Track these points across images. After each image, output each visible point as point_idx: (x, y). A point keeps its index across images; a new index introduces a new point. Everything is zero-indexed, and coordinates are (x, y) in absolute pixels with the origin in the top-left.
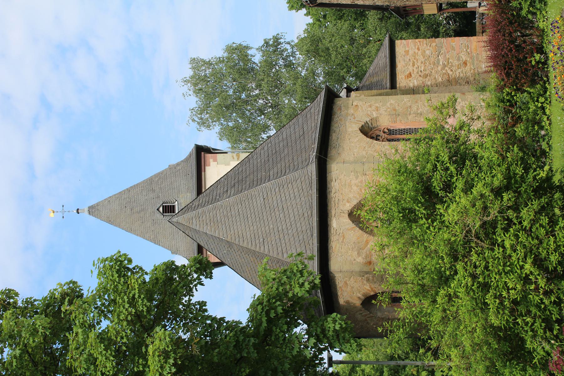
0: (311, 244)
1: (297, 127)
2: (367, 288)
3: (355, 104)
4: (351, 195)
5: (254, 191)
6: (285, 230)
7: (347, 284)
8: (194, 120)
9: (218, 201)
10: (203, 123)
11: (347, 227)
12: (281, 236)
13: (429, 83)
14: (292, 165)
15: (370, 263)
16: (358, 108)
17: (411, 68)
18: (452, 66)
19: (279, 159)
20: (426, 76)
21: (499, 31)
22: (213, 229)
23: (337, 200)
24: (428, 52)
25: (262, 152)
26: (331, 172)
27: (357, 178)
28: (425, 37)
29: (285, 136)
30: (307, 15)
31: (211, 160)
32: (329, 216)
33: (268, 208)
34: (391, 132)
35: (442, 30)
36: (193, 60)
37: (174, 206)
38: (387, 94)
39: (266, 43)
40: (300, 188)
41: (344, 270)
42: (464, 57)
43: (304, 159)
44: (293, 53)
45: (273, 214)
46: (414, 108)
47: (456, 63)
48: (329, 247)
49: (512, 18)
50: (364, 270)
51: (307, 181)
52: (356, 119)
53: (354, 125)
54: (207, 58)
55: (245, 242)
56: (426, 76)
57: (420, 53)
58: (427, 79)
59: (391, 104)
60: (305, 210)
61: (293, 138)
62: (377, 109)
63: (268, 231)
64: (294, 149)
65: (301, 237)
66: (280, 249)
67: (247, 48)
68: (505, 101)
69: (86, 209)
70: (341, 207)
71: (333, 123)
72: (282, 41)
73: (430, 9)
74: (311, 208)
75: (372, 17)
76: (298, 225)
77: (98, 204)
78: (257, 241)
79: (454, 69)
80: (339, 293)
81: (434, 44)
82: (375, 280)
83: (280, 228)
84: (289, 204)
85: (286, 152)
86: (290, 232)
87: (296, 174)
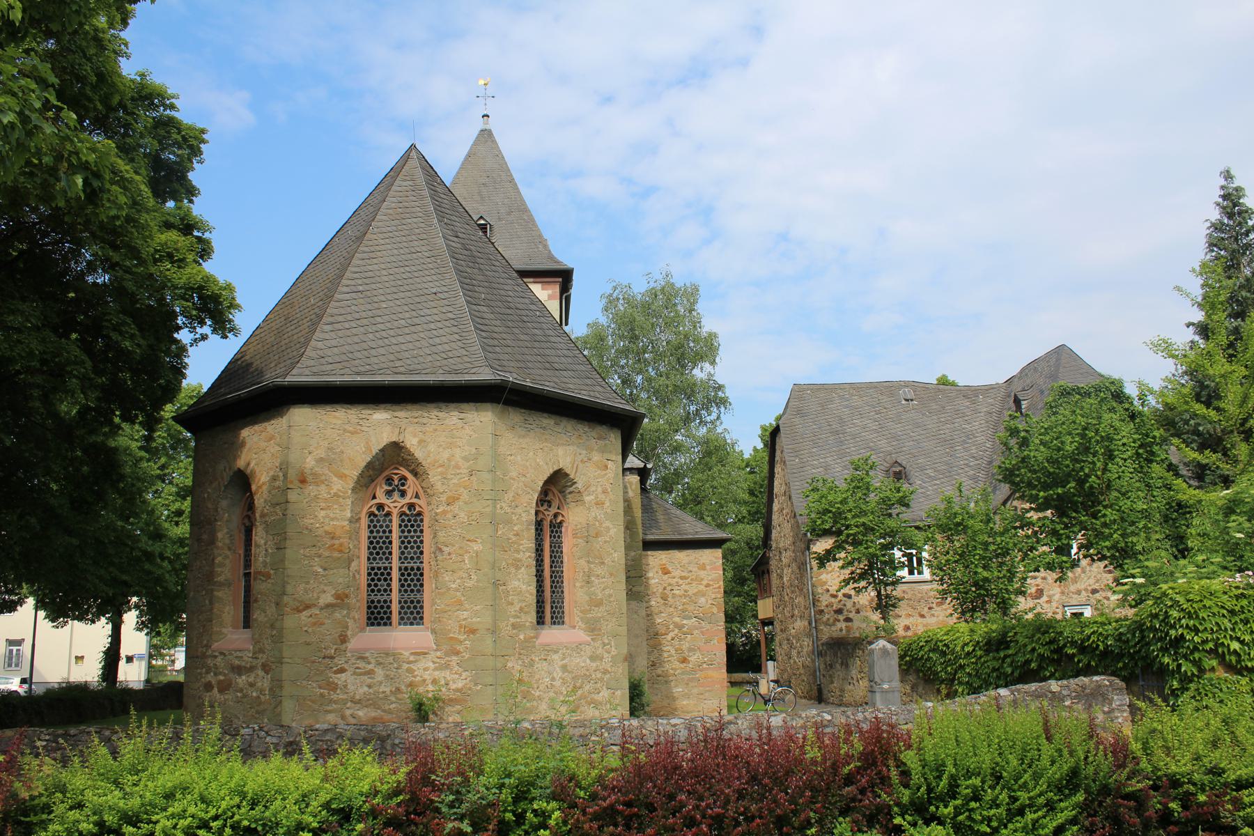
0: (342, 372)
1: (569, 360)
2: (262, 480)
4: (432, 448)
5: (452, 278)
6: (374, 328)
7: (271, 439)
8: (615, 288)
9: (439, 221)
10: (611, 302)
11: (373, 439)
12: (365, 322)
13: (653, 603)
14: (496, 342)
15: (303, 481)
16: (600, 475)
17: (677, 573)
18: (680, 640)
19: (510, 324)
20: (665, 598)
21: (754, 779)
22: (390, 211)
23: (425, 421)
24: (702, 600)
25: (527, 301)
26: (477, 410)
27: (466, 459)
28: (726, 603)
29: (553, 339)
30: (755, 449)
32: (394, 407)
33: (418, 300)
34: (556, 527)
35: (735, 626)
36: (696, 289)
38: (629, 526)
39: (720, 388)
40: (450, 354)
41: (293, 432)
42: (694, 658)
43: (505, 363)
44: (706, 423)
45: (406, 308)
46: (599, 570)
47: (685, 646)
48: (337, 406)
49: (796, 822)
50: (290, 471)
51: (461, 366)
52: (581, 465)
53: (568, 459)
54: (700, 307)
55: (361, 262)
56: (665, 598)
57: (702, 587)
58: (659, 600)
59: (608, 529)
60: (409, 362)
61: (548, 352)
62: (599, 504)
63: (375, 299)
64: (526, 351)
65: (358, 355)
66: (341, 319)
67: (713, 363)
68: (522, 805)
69: (487, 127)
70: (410, 429)
72: (722, 409)
73: (765, 608)
74: (411, 372)
75: (754, 531)
76: (382, 351)
77: (494, 142)
78: (360, 282)
79: (676, 642)
80: (256, 427)
81: (715, 610)
82: (274, 492)
83: (379, 319)
84: (422, 335)
85: (522, 337)
86: (371, 336)
87: (477, 348)
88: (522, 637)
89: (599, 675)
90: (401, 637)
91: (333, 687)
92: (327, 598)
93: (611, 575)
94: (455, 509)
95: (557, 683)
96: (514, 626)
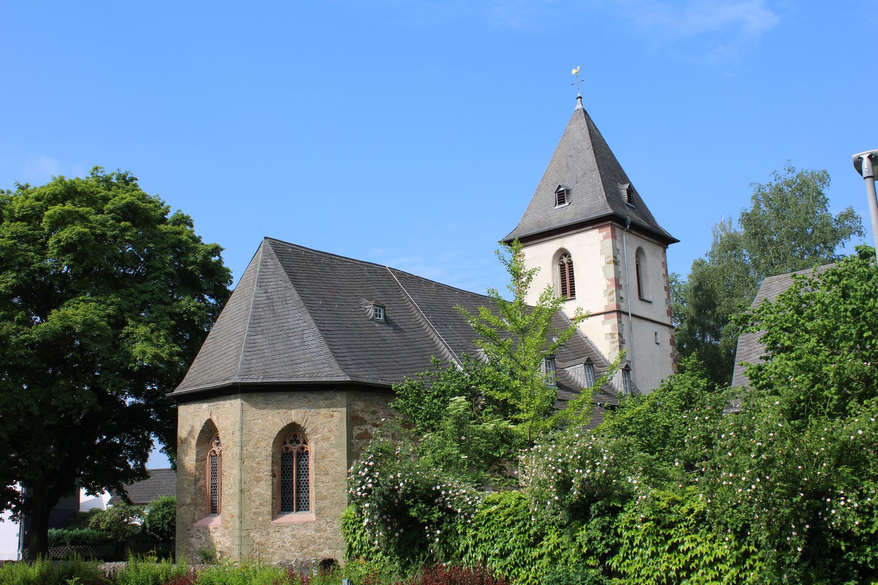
3: (335, 414)
27: (231, 425)
31: (605, 233)
34: (303, 454)
37: (564, 202)
46: (324, 479)
74: (199, 385)
88: (261, 519)
89: (322, 540)
90: (216, 521)
91: (190, 545)
92: (189, 501)
93: (334, 481)
94: (227, 452)
95: (288, 545)
96: (255, 513)
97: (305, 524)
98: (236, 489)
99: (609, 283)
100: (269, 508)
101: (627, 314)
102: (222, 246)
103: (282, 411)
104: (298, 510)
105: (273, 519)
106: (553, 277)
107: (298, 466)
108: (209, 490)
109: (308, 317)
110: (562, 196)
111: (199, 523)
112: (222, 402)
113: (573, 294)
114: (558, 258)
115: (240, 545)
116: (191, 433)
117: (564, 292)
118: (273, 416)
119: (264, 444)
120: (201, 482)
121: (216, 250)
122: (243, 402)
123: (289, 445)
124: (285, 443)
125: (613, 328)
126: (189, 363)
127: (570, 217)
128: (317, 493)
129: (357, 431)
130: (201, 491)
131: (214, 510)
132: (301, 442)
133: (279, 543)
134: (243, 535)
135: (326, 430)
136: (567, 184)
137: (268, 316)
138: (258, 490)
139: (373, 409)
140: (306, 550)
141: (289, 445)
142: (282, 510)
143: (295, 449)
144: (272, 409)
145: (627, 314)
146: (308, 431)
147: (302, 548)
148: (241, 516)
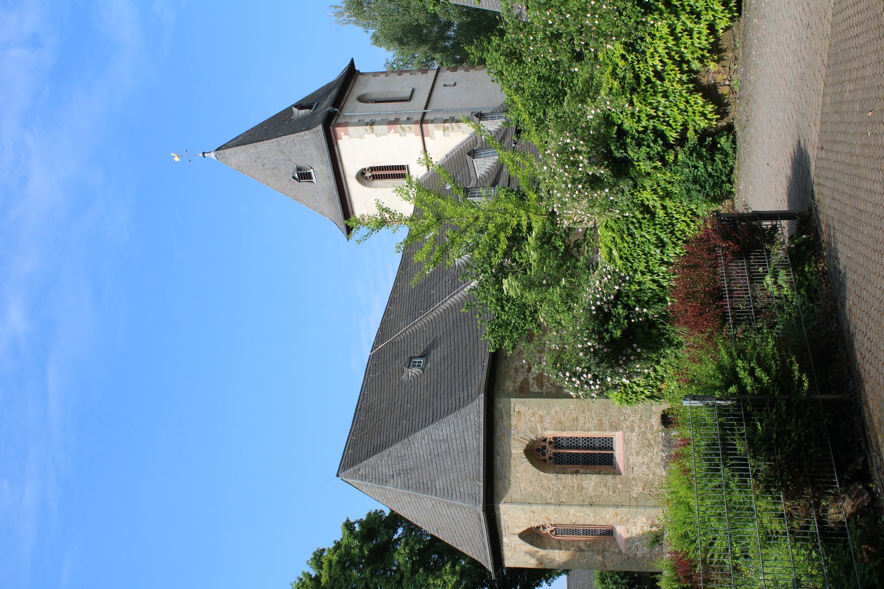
4: (521, 525)
27: (525, 514)
31: (342, 134)
34: (556, 442)
37: (310, 173)
46: (581, 421)
71: (496, 440)
89: (643, 425)
90: (621, 531)
91: (643, 557)
92: (600, 558)
94: (552, 518)
95: (646, 460)
97: (626, 442)
98: (589, 511)
99: (393, 131)
100: (609, 478)
101: (424, 114)
102: (345, 520)
103: (513, 462)
104: (612, 449)
105: (620, 474)
106: (385, 187)
107: (568, 447)
108: (590, 538)
109: (419, 434)
110: (304, 176)
111: (622, 547)
112: (502, 523)
113: (402, 167)
114: (366, 181)
115: (645, 507)
116: (532, 555)
117: (402, 176)
118: (517, 472)
119: (545, 481)
120: (582, 545)
121: (349, 526)
122: (503, 501)
123: (547, 457)
124: (545, 460)
125: (438, 128)
126: (463, 555)
127: (324, 168)
128: (595, 429)
129: (535, 388)
130: (590, 546)
131: (609, 533)
132: (544, 444)
133: (644, 468)
134: (635, 504)
135: (533, 419)
136: (292, 169)
137: (417, 475)
138: (591, 488)
139: (513, 371)
140: (652, 442)
141: (547, 457)
142: (612, 464)
143: (550, 451)
144: (510, 472)
145: (424, 114)
146: (533, 437)
147: (650, 445)
148: (616, 506)
